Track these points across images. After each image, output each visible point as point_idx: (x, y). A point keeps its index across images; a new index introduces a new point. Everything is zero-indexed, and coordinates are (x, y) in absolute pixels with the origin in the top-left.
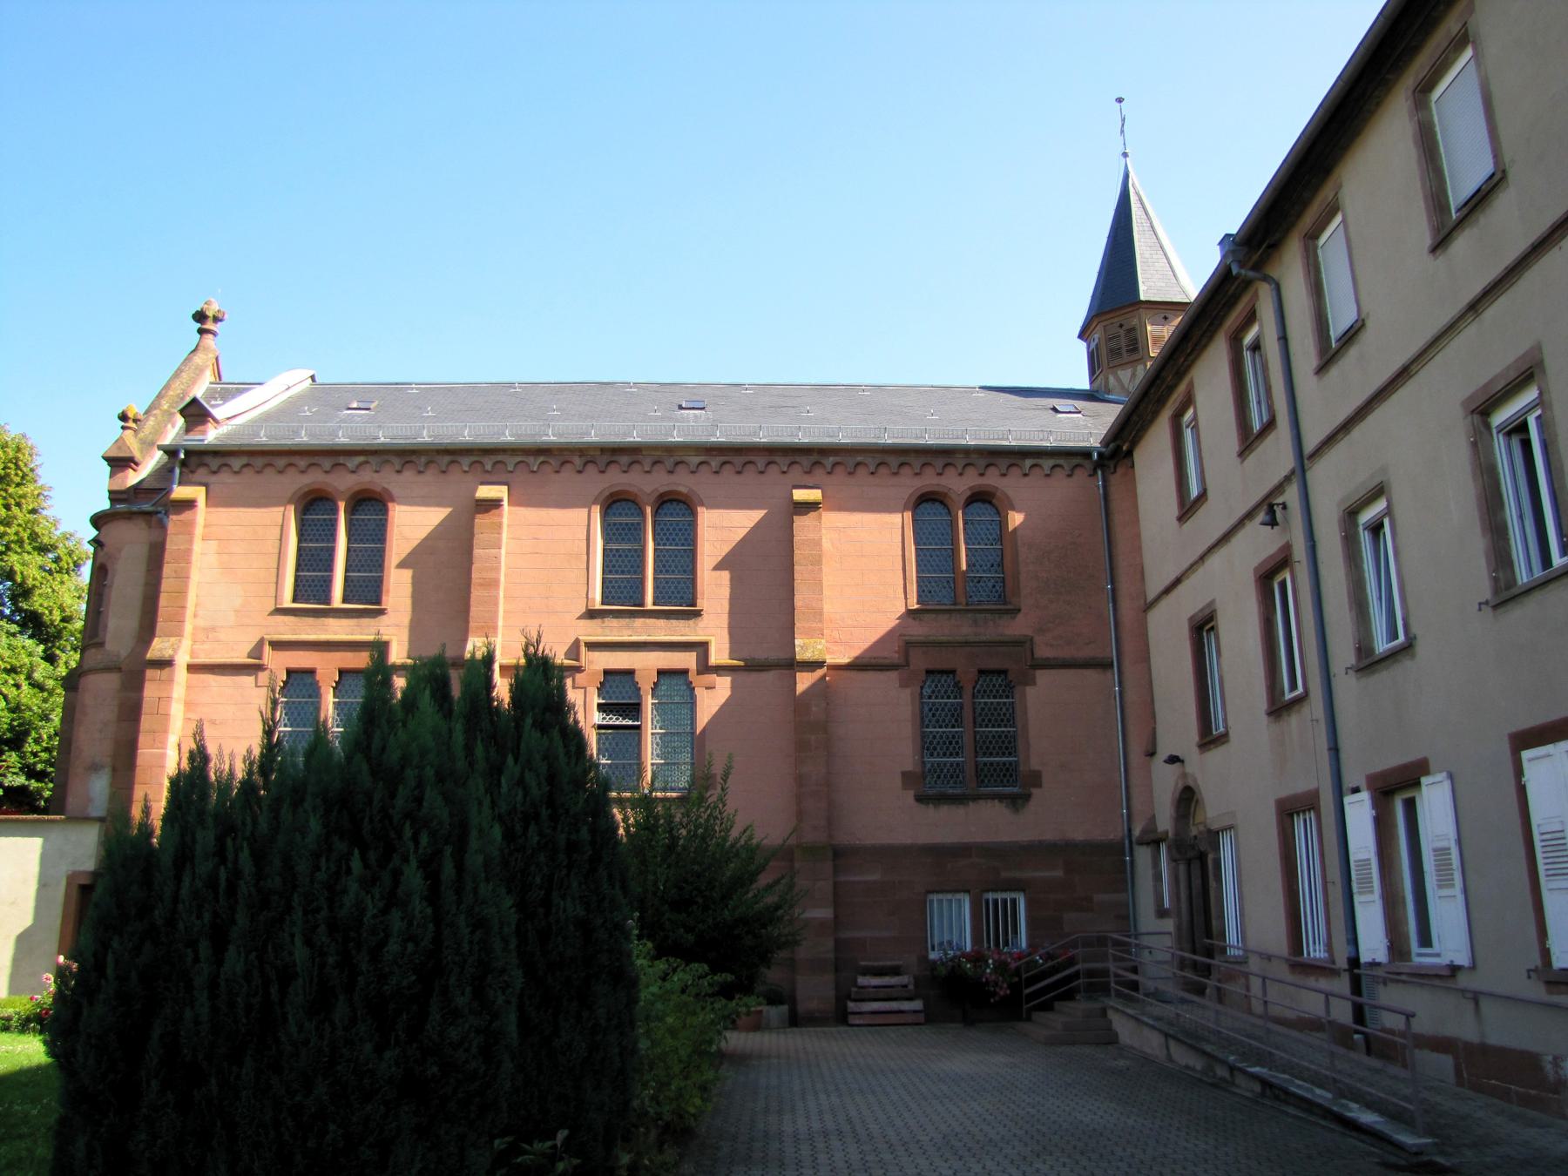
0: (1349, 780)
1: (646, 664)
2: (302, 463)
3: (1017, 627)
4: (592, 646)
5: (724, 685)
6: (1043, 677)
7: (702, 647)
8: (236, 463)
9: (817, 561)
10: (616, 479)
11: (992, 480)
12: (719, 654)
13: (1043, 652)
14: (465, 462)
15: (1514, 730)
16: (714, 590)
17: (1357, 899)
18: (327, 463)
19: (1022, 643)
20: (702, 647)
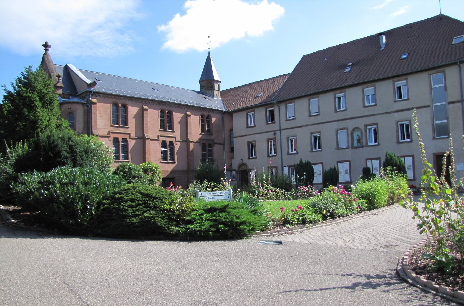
0: (284, 165)
1: (120, 137)
2: (113, 97)
3: (213, 137)
4: (161, 136)
5: (134, 141)
6: (216, 145)
7: (175, 137)
8: (101, 95)
9: (191, 125)
10: (162, 107)
11: (210, 114)
12: (178, 139)
13: (216, 142)
14: (140, 101)
15: (436, 152)
16: (132, 122)
17: (348, 169)
18: (117, 98)
19: (213, 140)
20: (129, 134)
